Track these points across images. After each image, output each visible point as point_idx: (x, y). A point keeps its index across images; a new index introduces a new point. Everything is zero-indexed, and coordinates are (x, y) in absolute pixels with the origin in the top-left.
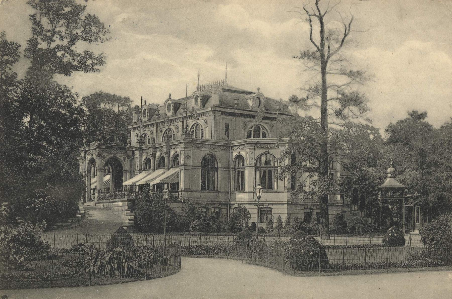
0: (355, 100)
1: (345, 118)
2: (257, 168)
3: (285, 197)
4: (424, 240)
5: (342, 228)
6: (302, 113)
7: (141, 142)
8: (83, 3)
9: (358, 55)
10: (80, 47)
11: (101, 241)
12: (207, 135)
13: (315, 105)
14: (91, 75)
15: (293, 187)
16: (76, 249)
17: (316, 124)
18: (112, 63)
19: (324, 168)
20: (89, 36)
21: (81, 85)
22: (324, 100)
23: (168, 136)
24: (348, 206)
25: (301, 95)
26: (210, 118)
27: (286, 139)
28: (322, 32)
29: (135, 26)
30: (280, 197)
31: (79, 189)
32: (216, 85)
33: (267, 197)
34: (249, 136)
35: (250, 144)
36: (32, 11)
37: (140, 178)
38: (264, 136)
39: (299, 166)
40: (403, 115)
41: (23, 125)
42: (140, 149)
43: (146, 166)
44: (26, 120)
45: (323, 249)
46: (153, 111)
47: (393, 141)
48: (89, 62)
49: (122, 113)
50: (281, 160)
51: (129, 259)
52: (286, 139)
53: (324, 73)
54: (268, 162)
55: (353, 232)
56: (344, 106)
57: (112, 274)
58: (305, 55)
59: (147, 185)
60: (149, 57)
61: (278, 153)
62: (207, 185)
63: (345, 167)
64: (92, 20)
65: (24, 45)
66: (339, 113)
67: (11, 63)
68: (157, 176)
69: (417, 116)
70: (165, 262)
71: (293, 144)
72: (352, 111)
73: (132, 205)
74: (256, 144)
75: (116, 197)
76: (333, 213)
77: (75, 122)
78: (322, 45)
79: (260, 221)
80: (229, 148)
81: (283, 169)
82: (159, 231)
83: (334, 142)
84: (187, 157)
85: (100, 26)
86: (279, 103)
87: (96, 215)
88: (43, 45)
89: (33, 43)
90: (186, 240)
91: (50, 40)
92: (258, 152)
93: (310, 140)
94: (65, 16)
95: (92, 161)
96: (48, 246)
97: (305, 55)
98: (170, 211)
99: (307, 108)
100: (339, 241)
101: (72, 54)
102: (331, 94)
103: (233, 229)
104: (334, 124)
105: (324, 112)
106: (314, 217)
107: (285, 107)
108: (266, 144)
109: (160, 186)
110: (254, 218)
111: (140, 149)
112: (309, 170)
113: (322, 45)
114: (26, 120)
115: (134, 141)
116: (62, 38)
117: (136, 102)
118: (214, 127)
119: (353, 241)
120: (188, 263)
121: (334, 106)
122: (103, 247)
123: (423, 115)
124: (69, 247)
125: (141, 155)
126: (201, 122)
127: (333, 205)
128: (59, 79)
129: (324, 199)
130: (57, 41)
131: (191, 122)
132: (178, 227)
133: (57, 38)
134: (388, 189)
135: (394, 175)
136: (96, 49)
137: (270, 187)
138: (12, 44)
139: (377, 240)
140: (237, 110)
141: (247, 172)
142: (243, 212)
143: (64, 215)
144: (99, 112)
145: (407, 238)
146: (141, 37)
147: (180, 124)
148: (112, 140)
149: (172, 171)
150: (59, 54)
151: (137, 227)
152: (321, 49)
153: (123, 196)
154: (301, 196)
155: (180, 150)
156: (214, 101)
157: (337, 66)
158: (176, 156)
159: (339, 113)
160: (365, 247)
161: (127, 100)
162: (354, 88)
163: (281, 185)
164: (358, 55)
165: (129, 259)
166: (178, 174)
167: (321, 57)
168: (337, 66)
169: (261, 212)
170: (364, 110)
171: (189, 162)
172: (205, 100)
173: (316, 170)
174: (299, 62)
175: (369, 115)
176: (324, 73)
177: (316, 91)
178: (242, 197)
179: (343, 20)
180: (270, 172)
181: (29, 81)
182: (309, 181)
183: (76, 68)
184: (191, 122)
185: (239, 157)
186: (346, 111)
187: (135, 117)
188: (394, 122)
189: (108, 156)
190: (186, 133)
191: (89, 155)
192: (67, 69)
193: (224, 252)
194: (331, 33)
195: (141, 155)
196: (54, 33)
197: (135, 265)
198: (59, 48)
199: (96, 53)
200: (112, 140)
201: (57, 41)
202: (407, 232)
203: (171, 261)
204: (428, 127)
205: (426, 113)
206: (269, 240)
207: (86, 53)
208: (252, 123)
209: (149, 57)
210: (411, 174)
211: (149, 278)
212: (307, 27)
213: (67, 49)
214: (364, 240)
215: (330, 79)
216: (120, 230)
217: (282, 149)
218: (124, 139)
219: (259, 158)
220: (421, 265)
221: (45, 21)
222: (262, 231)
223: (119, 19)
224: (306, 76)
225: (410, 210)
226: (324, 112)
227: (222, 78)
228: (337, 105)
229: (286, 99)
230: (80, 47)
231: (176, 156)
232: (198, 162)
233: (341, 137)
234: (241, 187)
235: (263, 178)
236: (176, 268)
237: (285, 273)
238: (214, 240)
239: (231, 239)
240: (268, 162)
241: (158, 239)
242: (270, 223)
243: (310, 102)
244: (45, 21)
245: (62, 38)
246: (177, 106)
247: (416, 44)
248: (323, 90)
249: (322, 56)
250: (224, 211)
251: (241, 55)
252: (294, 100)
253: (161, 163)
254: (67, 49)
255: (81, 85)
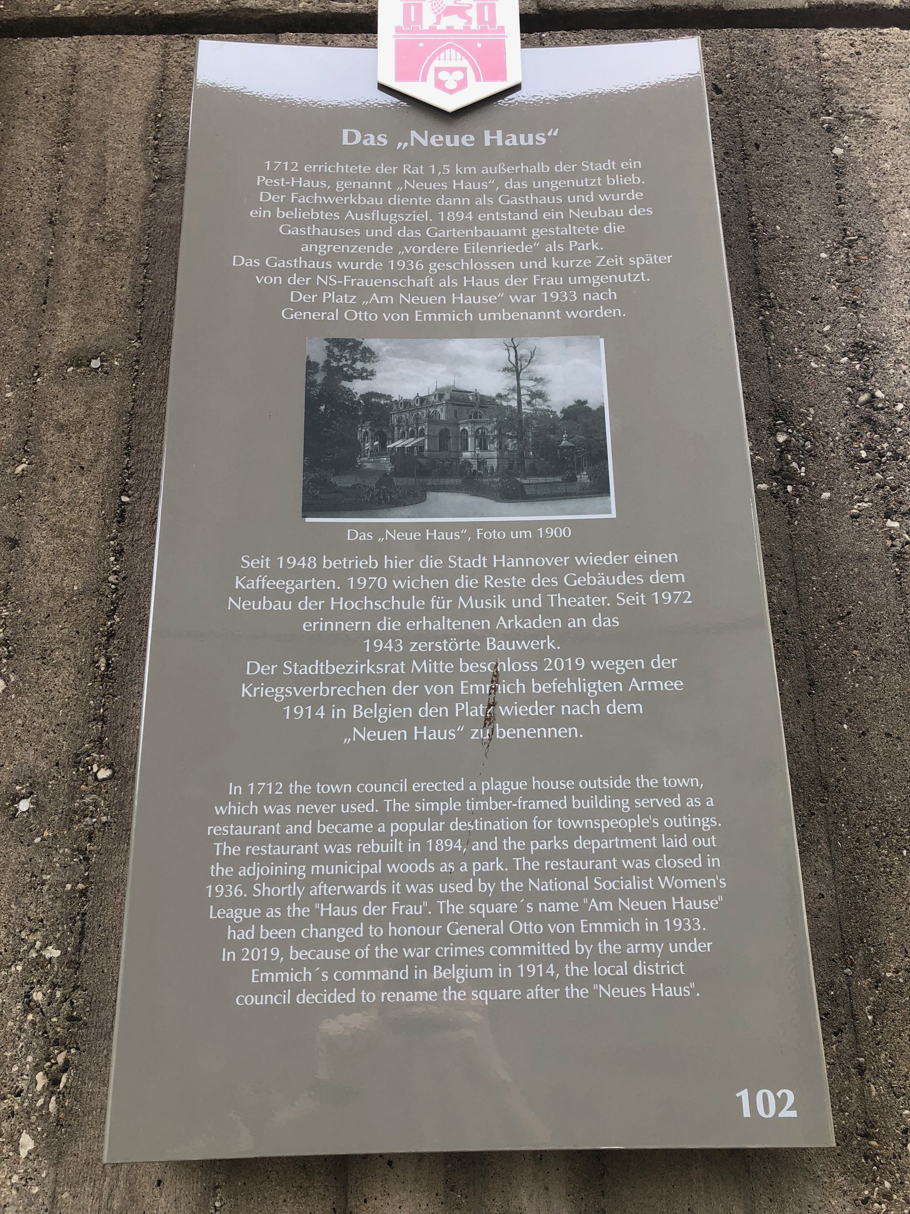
0: (540, 395)
1: (533, 405)
2: (476, 437)
3: (495, 454)
4: (590, 478)
5: (534, 472)
6: (505, 404)
7: (399, 421)
8: (361, 340)
9: (539, 369)
10: (359, 365)
11: (372, 482)
12: (443, 417)
13: (513, 398)
14: (366, 382)
15: (500, 448)
16: (354, 487)
17: (514, 410)
18: (379, 375)
19: (521, 437)
20: (364, 359)
21: (359, 387)
22: (519, 395)
23: (417, 418)
24: (538, 458)
25: (503, 393)
26: (444, 408)
27: (495, 419)
28: (516, 356)
29: (394, 354)
30: (492, 456)
31: (358, 449)
32: (448, 388)
33: (483, 454)
34: (470, 417)
35: (472, 422)
36: (327, 344)
37: (398, 444)
38: (480, 417)
39: (504, 435)
40: (572, 403)
41: (320, 410)
42: (398, 426)
43: (402, 436)
44: (322, 408)
45: (522, 485)
46: (407, 403)
47: (564, 418)
48: (365, 374)
49: (386, 404)
50: (492, 432)
51: (391, 493)
52: (495, 419)
53: (518, 379)
54: (483, 433)
55: (542, 474)
56: (532, 399)
57: (380, 503)
58: (506, 369)
59: (403, 447)
60: (404, 371)
61: (489, 428)
62: (443, 447)
63: (534, 434)
64: (367, 350)
65: (322, 364)
66: (529, 403)
67: (313, 374)
68: (410, 442)
69: (581, 403)
70: (415, 495)
71: (499, 422)
72: (538, 402)
73: (393, 461)
74: (475, 423)
75: (382, 455)
76: (527, 463)
77: (355, 410)
78: (517, 363)
79: (479, 469)
80: (458, 425)
81: (494, 437)
82: (411, 476)
83: (526, 419)
84: (429, 431)
85: (372, 353)
86: (490, 398)
87: (369, 466)
88: (335, 364)
89: (327, 363)
90: (430, 482)
91: (339, 361)
92: (477, 427)
93: (511, 419)
94: (349, 347)
95: (366, 433)
96: (336, 485)
97: (506, 369)
98: (419, 463)
99: (509, 400)
100: (533, 480)
101: (353, 369)
102: (523, 391)
103: (461, 474)
104: (526, 409)
105: (519, 402)
106: (515, 465)
107: (494, 400)
108: (482, 422)
109: (412, 448)
110: (475, 467)
111: (398, 426)
112: (510, 437)
113: (517, 363)
114: (322, 408)
115: (394, 420)
116: (347, 360)
117: (396, 398)
118: (447, 412)
119: (542, 480)
120: (431, 495)
121: (525, 398)
122: (374, 486)
123: (586, 402)
124: (350, 485)
125: (399, 429)
126: (438, 410)
127: (528, 458)
128: (345, 384)
129: (521, 455)
130: (344, 362)
131: (432, 410)
132: (423, 473)
133: (343, 360)
134: (564, 447)
135: (567, 439)
136: (369, 367)
137: (485, 449)
138: (314, 363)
139: (559, 479)
140: (462, 402)
141: (469, 439)
142: (467, 463)
143: (348, 465)
144: (371, 404)
145: (578, 477)
146: (398, 360)
147: (424, 411)
148: (379, 420)
149: (419, 439)
150: (345, 369)
151: (396, 473)
152: (516, 366)
153: (386, 454)
154: (506, 453)
155: (425, 426)
156: (447, 396)
157: (527, 376)
158: (422, 430)
159: (529, 403)
160: (550, 483)
161: (390, 396)
162: (539, 388)
163: (493, 446)
164: (539, 369)
165: (391, 493)
166: (424, 441)
167: (516, 370)
168: (527, 376)
169: (479, 464)
170: (546, 401)
171: (431, 434)
172: (441, 396)
173: (516, 437)
174: (502, 374)
175: (549, 403)
176: (518, 379)
177: (513, 390)
178: (466, 455)
179: (529, 349)
180: (485, 440)
181: (323, 384)
182: (511, 444)
183: (356, 378)
184: (432, 410)
185: (464, 430)
186: (534, 402)
187: (395, 407)
188: (566, 407)
189: (377, 430)
190: (429, 416)
191: (363, 430)
192: (350, 378)
193: (456, 489)
194: (522, 357)
195: (399, 429)
196: (342, 357)
197: (395, 496)
198: (345, 366)
199: (369, 369)
200: (379, 420)
201: (344, 362)
202: (578, 473)
203: (419, 494)
204: (589, 409)
205: (549, 382)
206: (486, 480)
207: (363, 369)
208: (473, 410)
209: (404, 371)
210: (579, 437)
211: (405, 505)
212: (506, 353)
213: (350, 367)
214: (550, 479)
215: (522, 383)
216: (385, 475)
217: (492, 425)
218: (388, 420)
219: (477, 431)
220: (589, 494)
221: (336, 350)
222: (480, 475)
223: (384, 349)
224: (507, 381)
225: (579, 460)
226: (519, 402)
227: (451, 384)
228: (528, 398)
229: (494, 395)
230: (359, 365)
231: (422, 430)
232: (437, 433)
233: (530, 417)
234: (466, 449)
235: (480, 444)
236: (423, 499)
237: (497, 501)
238: (448, 481)
239: (460, 481)
240: (483, 433)
241: (411, 481)
242: (486, 470)
243: (510, 397)
244: (336, 350)
245: (347, 360)
246: (422, 400)
247: (577, 361)
248: (518, 389)
249: (517, 370)
250: (454, 463)
251: (463, 370)
252: (499, 396)
253: (412, 435)
254: (350, 367)
255: (359, 387)
